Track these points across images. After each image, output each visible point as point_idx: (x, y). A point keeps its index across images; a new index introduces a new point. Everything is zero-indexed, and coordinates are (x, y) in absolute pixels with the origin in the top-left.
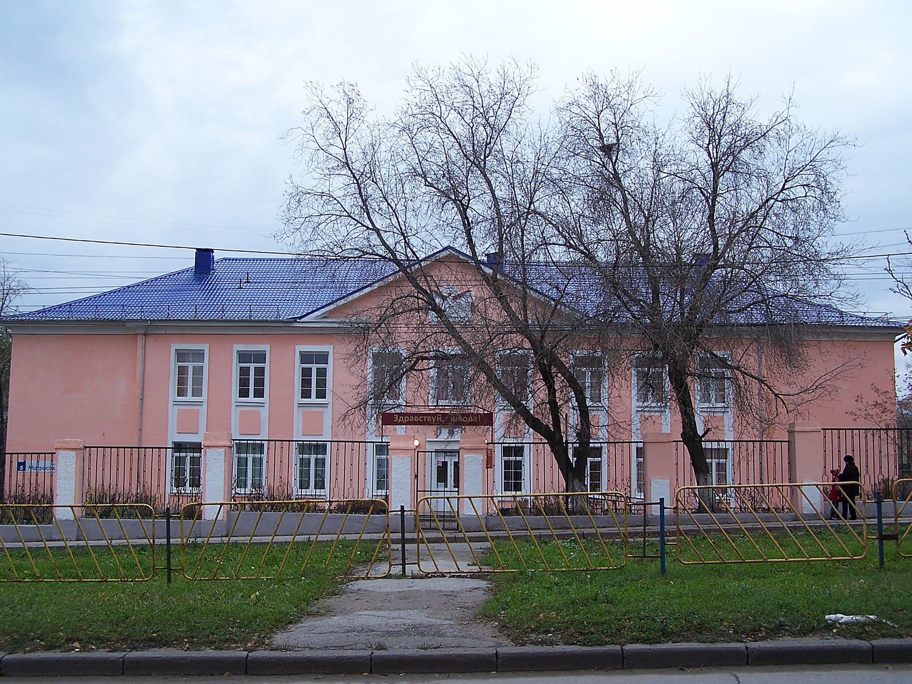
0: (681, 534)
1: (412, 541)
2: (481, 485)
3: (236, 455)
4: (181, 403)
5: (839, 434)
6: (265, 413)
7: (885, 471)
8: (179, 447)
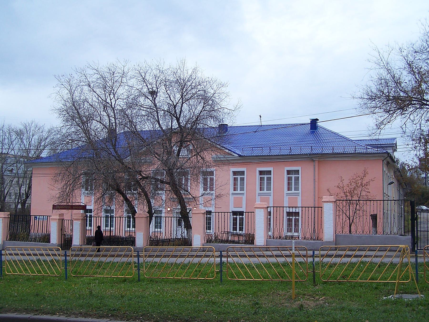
0: (7, 255)
1: (225, 257)
2: (79, 233)
3: (232, 216)
4: (234, 194)
5: (96, 219)
6: (244, 197)
7: (167, 235)
8: (235, 213)
